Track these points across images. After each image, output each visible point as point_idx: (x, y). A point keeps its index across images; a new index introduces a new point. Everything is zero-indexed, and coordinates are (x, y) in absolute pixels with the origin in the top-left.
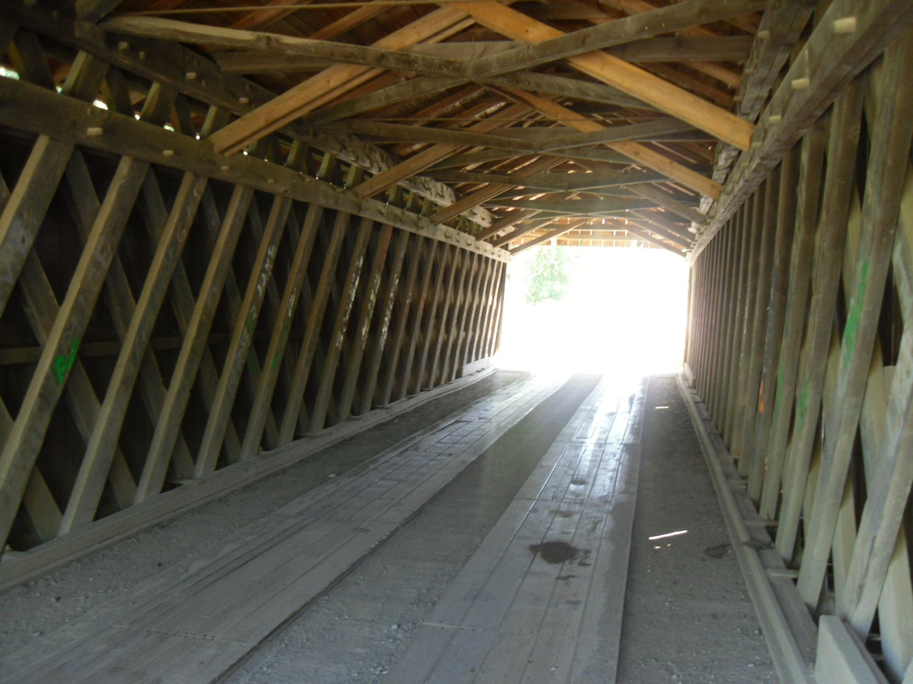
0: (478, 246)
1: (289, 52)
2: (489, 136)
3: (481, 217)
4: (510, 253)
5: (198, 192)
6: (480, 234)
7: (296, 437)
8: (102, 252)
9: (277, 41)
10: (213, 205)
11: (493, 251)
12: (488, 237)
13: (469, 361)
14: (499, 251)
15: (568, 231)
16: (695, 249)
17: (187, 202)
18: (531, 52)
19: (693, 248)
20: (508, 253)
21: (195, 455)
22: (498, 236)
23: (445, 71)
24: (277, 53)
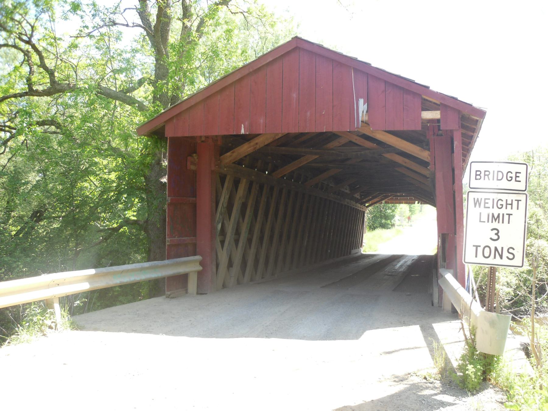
3: (357, 196)
6: (357, 201)
12: (360, 202)
13: (353, 249)
20: (409, 209)
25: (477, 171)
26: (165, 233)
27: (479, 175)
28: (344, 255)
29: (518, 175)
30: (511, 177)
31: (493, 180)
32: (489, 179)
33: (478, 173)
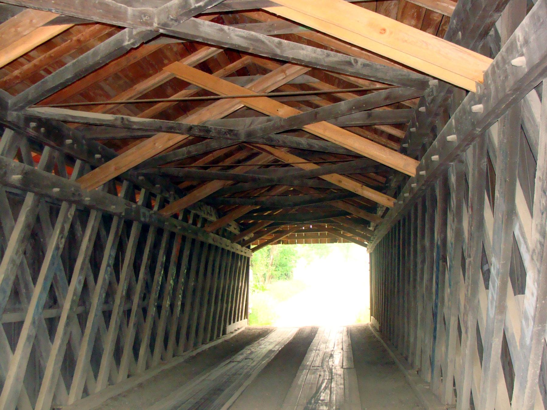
0: (233, 247)
1: (135, 127)
2: (246, 175)
4: (251, 251)
5: (70, 214)
6: (233, 238)
7: (174, 356)
8: (17, 254)
9: (128, 120)
10: (78, 223)
11: (241, 250)
13: (230, 324)
14: (246, 249)
15: (288, 235)
16: (374, 241)
17: (65, 222)
18: (282, 123)
19: (373, 240)
21: (68, 387)
22: (244, 240)
23: (228, 136)
24: (128, 127)
26: (529, 195)
28: (211, 340)
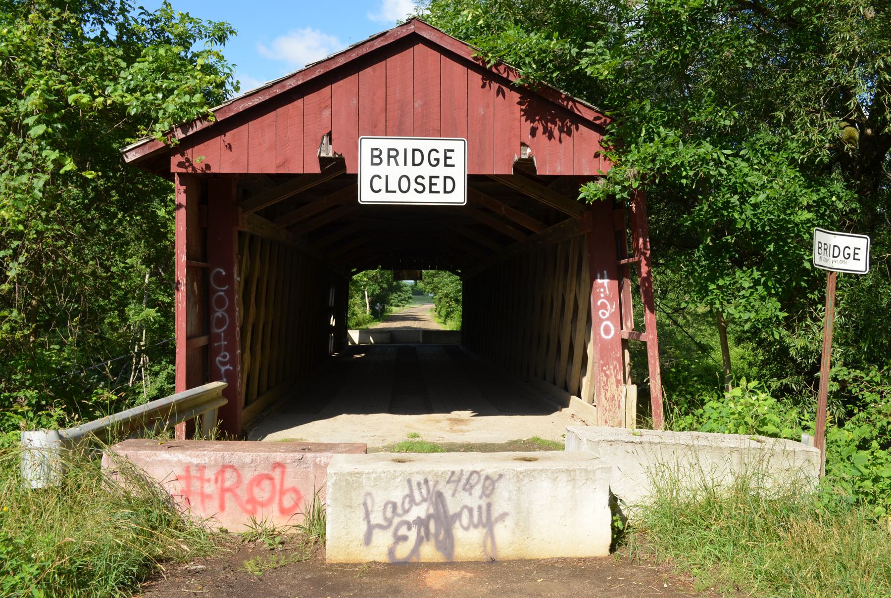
25: (373, 150)
27: (378, 156)
29: (449, 154)
30: (438, 160)
31: (405, 164)
32: (397, 164)
33: (376, 153)
